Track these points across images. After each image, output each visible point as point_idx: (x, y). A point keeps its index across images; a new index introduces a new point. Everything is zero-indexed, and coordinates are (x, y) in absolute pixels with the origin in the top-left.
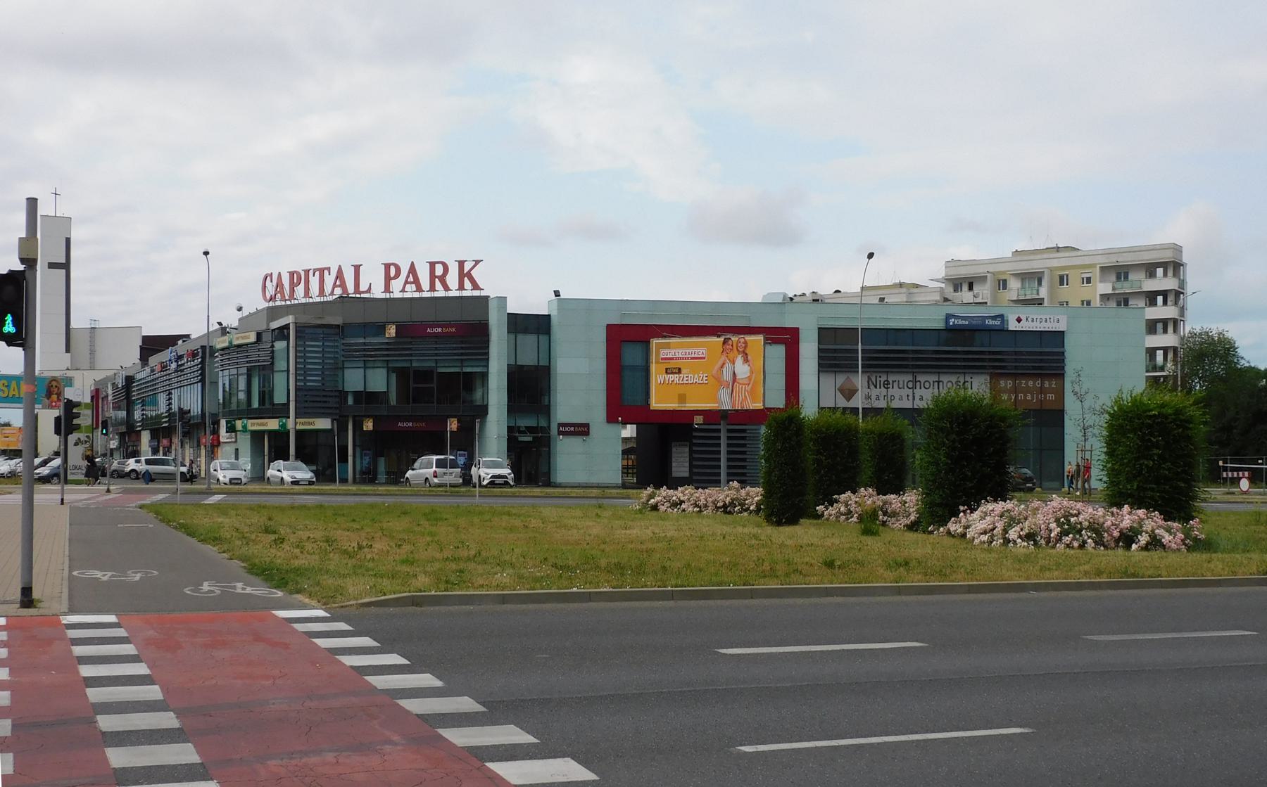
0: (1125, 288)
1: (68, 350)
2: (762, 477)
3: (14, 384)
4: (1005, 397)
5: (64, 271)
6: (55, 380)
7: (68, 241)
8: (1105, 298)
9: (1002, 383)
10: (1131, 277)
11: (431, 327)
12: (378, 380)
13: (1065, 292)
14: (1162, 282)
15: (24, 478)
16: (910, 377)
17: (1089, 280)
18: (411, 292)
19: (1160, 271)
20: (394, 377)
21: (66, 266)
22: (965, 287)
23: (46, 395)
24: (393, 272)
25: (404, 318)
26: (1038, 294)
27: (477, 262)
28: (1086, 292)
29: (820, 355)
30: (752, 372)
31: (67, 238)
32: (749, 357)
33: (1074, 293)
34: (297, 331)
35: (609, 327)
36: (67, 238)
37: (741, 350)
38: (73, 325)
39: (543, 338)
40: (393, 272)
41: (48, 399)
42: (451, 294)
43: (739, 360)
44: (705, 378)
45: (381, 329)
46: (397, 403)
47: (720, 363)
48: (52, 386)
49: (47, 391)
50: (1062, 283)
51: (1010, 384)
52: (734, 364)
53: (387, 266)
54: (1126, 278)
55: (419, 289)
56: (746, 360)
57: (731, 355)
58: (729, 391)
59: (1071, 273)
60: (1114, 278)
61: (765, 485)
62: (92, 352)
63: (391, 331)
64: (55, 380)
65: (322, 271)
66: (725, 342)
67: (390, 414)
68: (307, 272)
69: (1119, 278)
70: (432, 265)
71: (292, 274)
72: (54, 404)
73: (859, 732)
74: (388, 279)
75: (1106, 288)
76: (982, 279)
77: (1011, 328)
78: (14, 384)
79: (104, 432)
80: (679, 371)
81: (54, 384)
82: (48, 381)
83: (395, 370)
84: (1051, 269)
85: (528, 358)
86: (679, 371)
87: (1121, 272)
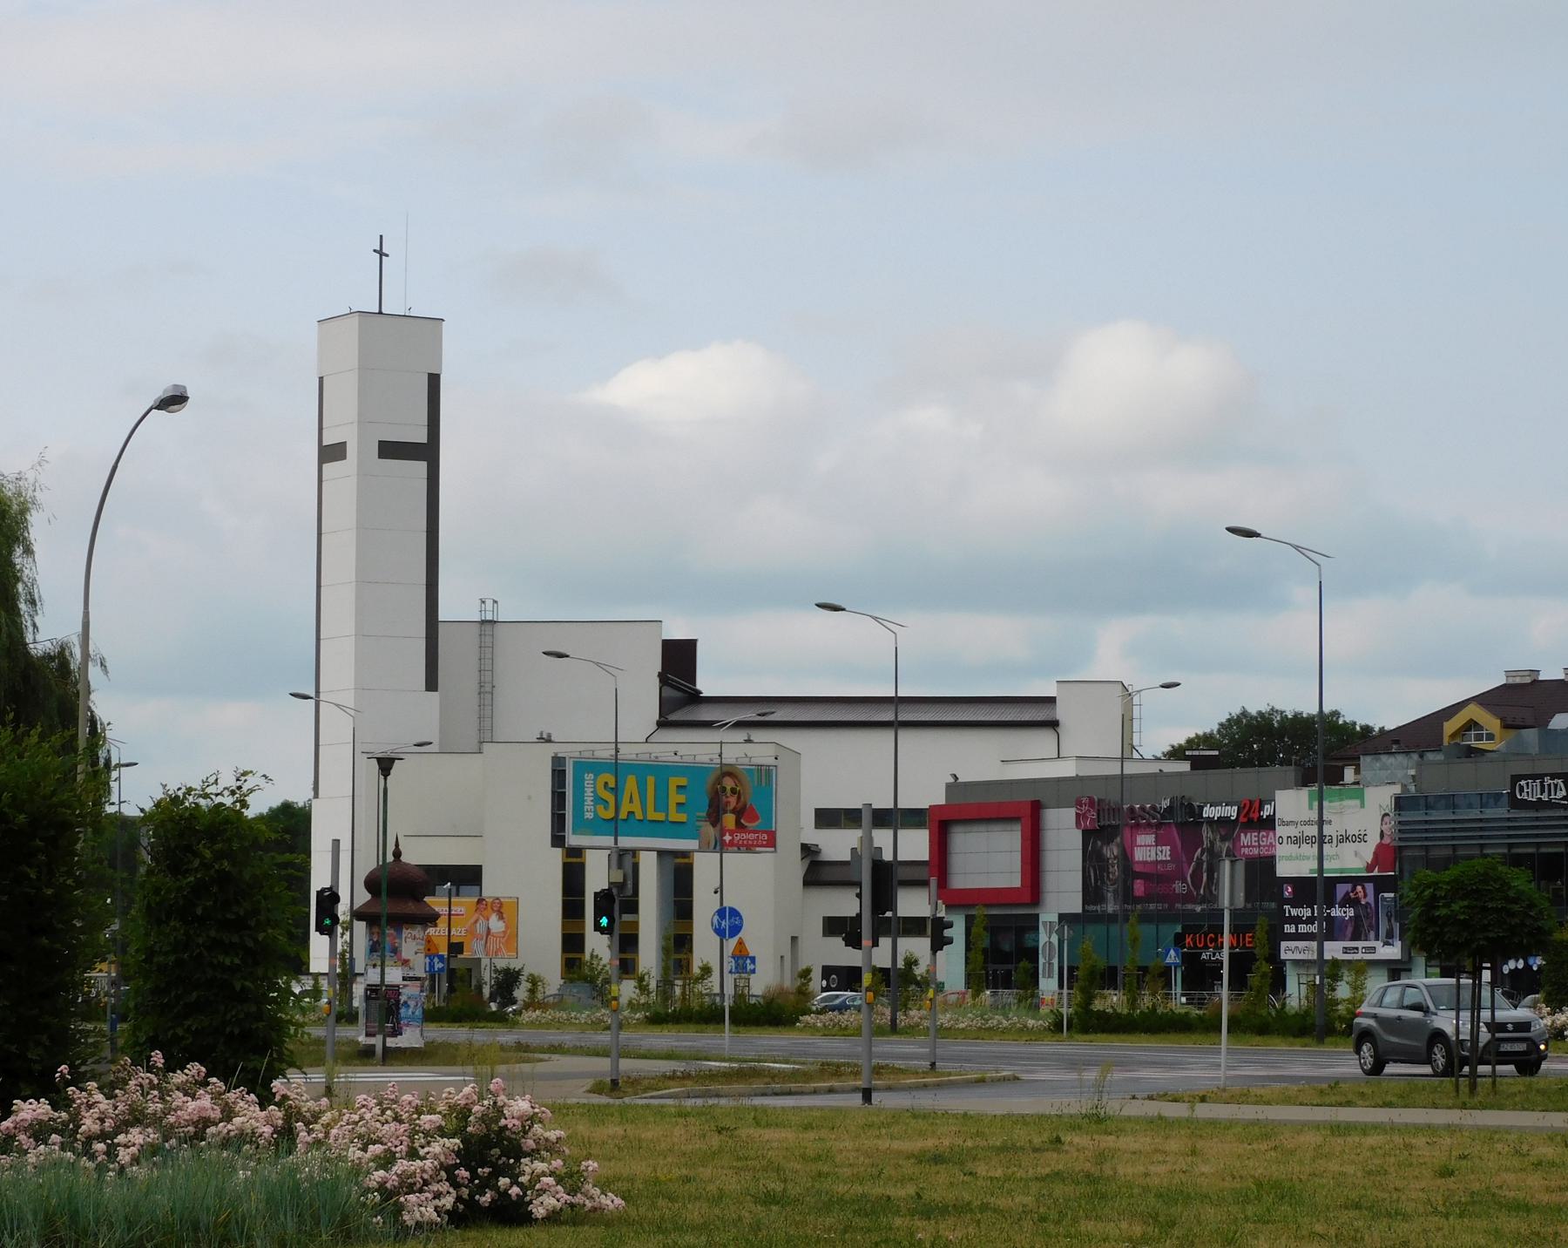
1: (432, 684)
2: (92, 1011)
5: (421, 467)
6: (730, 774)
7: (434, 381)
15: (865, 1030)
21: (428, 452)
23: (709, 815)
29: (307, 910)
30: (507, 927)
31: (430, 375)
32: (504, 916)
36: (430, 375)
37: (495, 909)
38: (443, 615)
41: (714, 825)
43: (494, 918)
44: (463, 932)
46: (1454, 978)
47: (472, 920)
48: (724, 789)
49: (710, 806)
52: (488, 920)
56: (501, 917)
57: (485, 913)
58: (483, 942)
64: (730, 774)
72: (727, 838)
73: (1339, 1237)
79: (604, 921)
81: (729, 783)
82: (712, 778)
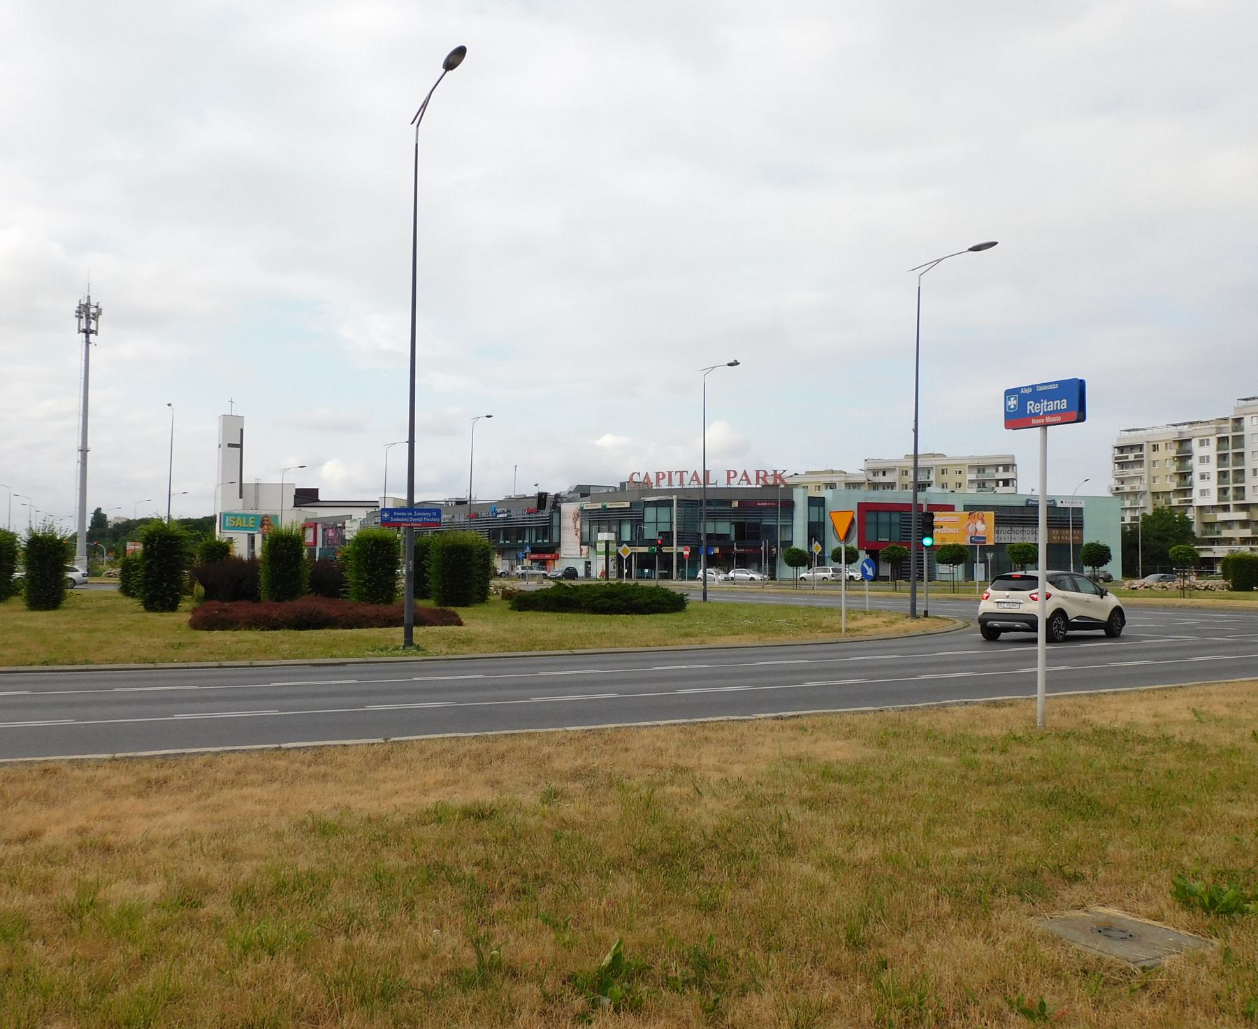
0: (982, 477)
1: (241, 497)
3: (239, 518)
4: (1055, 538)
7: (242, 430)
8: (971, 481)
9: (1054, 531)
10: (986, 471)
11: (760, 502)
12: (724, 528)
13: (945, 479)
14: (1001, 475)
16: (1009, 529)
17: (960, 472)
18: (744, 485)
19: (1001, 469)
20: (733, 526)
21: (240, 446)
22: (881, 474)
24: (732, 474)
25: (743, 497)
26: (928, 478)
27: (784, 471)
28: (959, 478)
33: (951, 479)
34: (677, 503)
35: (859, 503)
39: (822, 509)
40: (732, 474)
42: (752, 486)
45: (729, 503)
50: (943, 473)
51: (1057, 532)
53: (729, 472)
54: (984, 471)
55: (749, 483)
59: (949, 468)
60: (976, 472)
61: (69, 558)
62: (257, 499)
63: (736, 504)
65: (681, 473)
66: (970, 514)
67: (925, 552)
68: (670, 473)
69: (979, 472)
70: (758, 472)
71: (658, 474)
74: (729, 477)
75: (973, 476)
76: (892, 470)
77: (1058, 506)
78: (239, 518)
80: (942, 527)
81: (266, 519)
83: (732, 523)
84: (936, 466)
85: (815, 519)
86: (942, 527)
87: (981, 469)
